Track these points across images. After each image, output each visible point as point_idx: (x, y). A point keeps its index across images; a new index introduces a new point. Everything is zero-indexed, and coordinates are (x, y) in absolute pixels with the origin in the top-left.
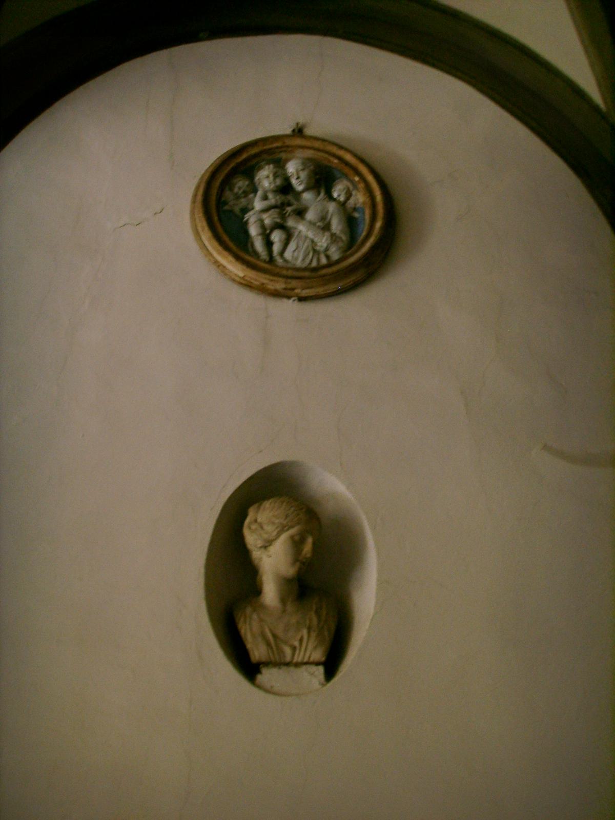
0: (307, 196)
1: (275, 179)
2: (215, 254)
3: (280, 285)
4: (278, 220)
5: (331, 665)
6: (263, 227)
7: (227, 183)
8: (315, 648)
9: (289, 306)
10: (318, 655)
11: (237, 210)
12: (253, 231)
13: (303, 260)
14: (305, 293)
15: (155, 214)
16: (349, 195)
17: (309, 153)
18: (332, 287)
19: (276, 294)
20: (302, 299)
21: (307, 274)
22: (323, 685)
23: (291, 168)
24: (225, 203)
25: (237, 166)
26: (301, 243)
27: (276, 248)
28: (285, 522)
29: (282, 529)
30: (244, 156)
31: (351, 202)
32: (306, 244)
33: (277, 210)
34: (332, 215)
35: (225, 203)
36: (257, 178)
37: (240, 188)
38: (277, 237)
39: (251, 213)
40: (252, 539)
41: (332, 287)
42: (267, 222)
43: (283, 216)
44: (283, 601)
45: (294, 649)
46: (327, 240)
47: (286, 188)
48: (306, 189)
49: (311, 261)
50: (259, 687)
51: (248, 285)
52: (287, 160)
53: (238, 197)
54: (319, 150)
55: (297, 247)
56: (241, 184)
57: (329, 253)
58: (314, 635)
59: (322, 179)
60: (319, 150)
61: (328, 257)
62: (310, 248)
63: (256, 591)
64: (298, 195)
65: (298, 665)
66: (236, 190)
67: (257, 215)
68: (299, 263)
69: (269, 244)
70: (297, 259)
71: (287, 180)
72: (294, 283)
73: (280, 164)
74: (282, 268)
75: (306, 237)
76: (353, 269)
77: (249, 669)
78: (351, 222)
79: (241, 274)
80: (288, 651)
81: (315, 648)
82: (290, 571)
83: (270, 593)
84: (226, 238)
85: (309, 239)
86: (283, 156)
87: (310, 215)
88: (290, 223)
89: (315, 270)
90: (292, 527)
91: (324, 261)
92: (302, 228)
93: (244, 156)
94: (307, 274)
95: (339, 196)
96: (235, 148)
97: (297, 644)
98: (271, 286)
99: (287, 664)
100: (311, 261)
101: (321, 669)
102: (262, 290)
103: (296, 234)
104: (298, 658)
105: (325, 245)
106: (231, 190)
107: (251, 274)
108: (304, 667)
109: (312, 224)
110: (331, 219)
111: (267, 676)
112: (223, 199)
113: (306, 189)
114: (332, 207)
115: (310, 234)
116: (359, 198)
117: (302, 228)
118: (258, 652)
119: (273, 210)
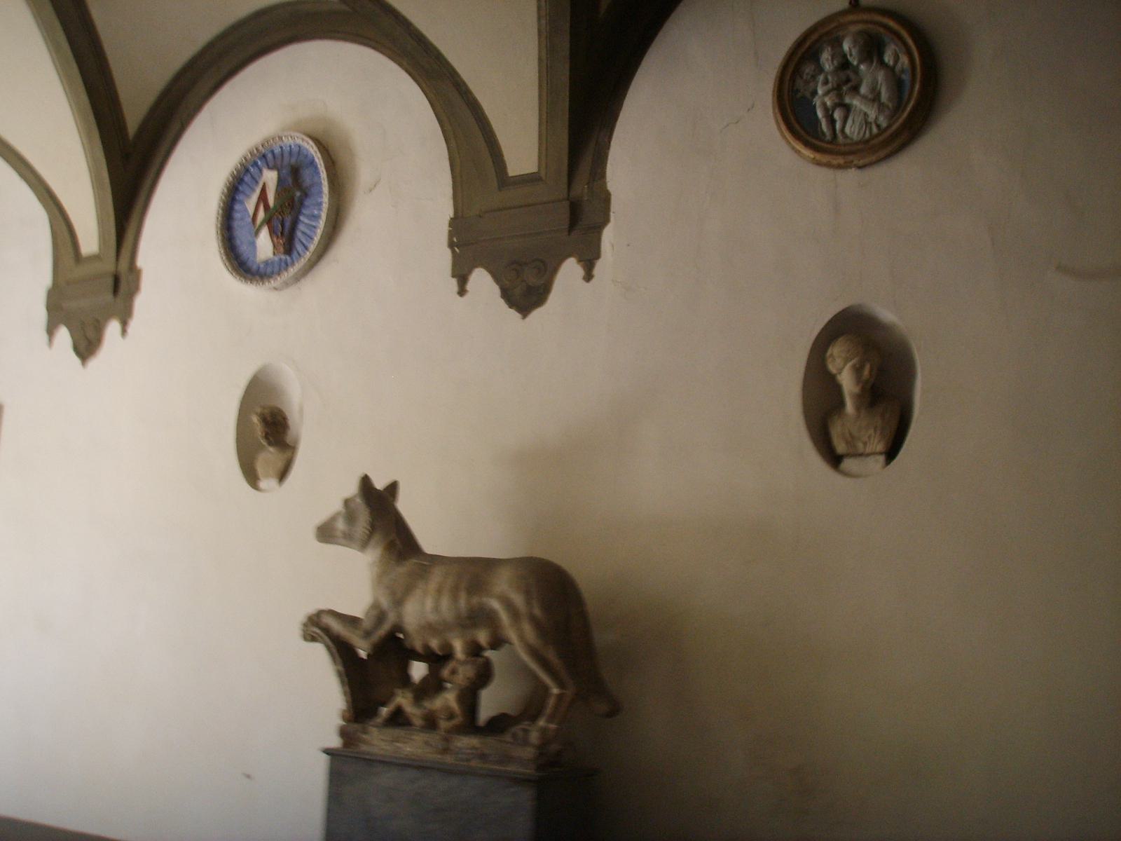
0: (862, 67)
1: (832, 61)
2: (792, 142)
3: (841, 160)
4: (837, 101)
5: (891, 453)
6: (826, 109)
7: (797, 72)
8: (880, 441)
9: (852, 173)
10: (880, 447)
11: (808, 95)
12: (820, 114)
13: (859, 133)
14: (861, 162)
15: (749, 110)
16: (897, 59)
17: (860, 27)
18: (882, 154)
19: (839, 167)
20: (860, 167)
21: (860, 147)
22: (884, 467)
23: (846, 46)
24: (798, 91)
25: (802, 57)
26: (856, 119)
27: (838, 126)
28: (848, 355)
29: (846, 360)
30: (808, 44)
31: (899, 65)
32: (860, 119)
33: (835, 92)
34: (881, 84)
35: (798, 91)
36: (821, 60)
37: (807, 74)
38: (837, 115)
39: (817, 97)
40: (832, 368)
41: (889, 149)
42: (829, 103)
43: (840, 96)
44: (858, 409)
45: (865, 444)
46: (875, 111)
47: (845, 65)
48: (860, 62)
49: (865, 132)
50: (846, 474)
51: (819, 164)
52: (844, 37)
53: (807, 82)
54: (866, 22)
55: (853, 121)
56: (808, 69)
57: (879, 122)
58: (878, 432)
59: (872, 48)
60: (866, 22)
61: (878, 126)
62: (863, 122)
63: (841, 404)
64: (856, 70)
65: (868, 455)
66: (805, 78)
67: (822, 98)
68: (855, 137)
69: (832, 122)
70: (854, 132)
71: (845, 56)
72: (851, 158)
73: (837, 43)
74: (845, 145)
75: (861, 110)
76: (905, 126)
77: (835, 460)
78: (898, 85)
79: (812, 156)
80: (860, 446)
81: (880, 441)
82: (856, 390)
83: (850, 407)
84: (797, 127)
85: (862, 117)
86: (840, 33)
87: (863, 90)
88: (847, 100)
89: (867, 141)
90: (853, 359)
91: (875, 130)
92: (856, 102)
93: (808, 44)
94: (860, 147)
95: (889, 61)
96: (784, 58)
97: (867, 439)
98: (835, 162)
99: (861, 455)
100: (865, 132)
101: (882, 459)
102: (829, 165)
103: (853, 109)
104: (868, 450)
105: (874, 117)
106: (802, 77)
107: (818, 156)
108: (872, 456)
109: (864, 97)
110: (880, 89)
111: (848, 464)
112: (795, 88)
113: (860, 62)
114: (881, 76)
115: (864, 108)
116: (904, 60)
117: (856, 102)
118: (840, 448)
119: (832, 93)
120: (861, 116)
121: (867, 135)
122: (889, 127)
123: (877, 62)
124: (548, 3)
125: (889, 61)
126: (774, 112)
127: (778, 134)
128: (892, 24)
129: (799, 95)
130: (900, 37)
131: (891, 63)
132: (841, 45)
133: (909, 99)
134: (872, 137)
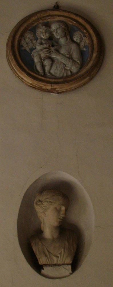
3: (49, 87)
5: (75, 266)
10: (69, 261)
23: (54, 27)
25: (26, 27)
33: (78, 43)
43: (50, 52)
47: (51, 38)
51: (34, 87)
61: (71, 72)
69: (43, 67)
72: (55, 86)
73: (48, 25)
77: (38, 267)
78: (82, 53)
85: (62, 64)
87: (63, 51)
88: (53, 56)
91: (69, 73)
93: (31, 21)
95: (77, 40)
101: (70, 267)
111: (46, 271)
116: (86, 40)
120: (62, 65)
121: (65, 75)
122: (78, 72)
123: (70, 39)
124: (35, 69)
125: (77, 40)
126: (7, 55)
127: (8, 68)
128: (81, 20)
129: (23, 49)
130: (85, 29)
131: (78, 41)
132: (50, 27)
133: (90, 61)
134: (67, 76)
